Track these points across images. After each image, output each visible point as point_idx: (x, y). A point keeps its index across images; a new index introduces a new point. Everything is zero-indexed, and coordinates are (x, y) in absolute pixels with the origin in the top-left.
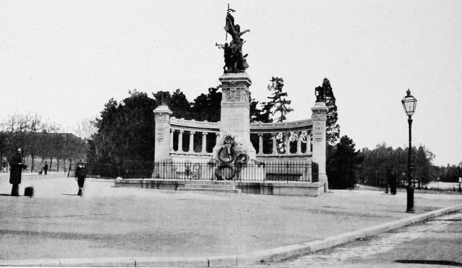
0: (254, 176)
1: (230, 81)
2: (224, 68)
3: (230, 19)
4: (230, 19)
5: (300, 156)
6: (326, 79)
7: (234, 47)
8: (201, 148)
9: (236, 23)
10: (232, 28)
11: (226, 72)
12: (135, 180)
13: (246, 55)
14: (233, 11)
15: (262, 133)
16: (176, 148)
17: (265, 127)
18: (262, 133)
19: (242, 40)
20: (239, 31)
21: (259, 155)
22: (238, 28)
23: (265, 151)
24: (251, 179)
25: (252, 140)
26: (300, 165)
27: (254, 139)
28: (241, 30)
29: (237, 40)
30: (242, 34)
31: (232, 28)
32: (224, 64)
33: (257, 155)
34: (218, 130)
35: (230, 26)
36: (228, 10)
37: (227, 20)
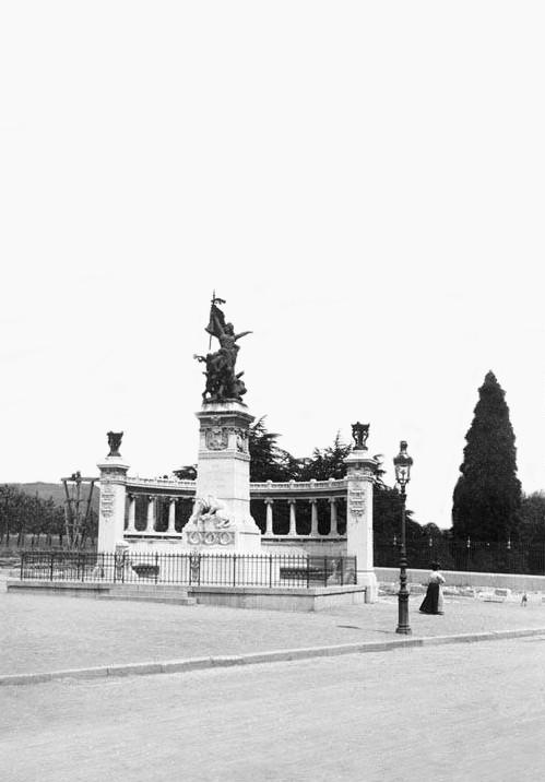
0: (219, 575)
1: (212, 417)
2: (204, 395)
3: (217, 315)
4: (217, 315)
5: (335, 540)
6: (490, 378)
7: (220, 361)
8: (146, 524)
9: (227, 321)
10: (218, 325)
11: (206, 402)
12: (352, 641)
13: (241, 374)
14: (221, 301)
15: (294, 499)
16: (141, 523)
17: (320, 488)
18: (294, 499)
19: (237, 348)
20: (232, 334)
21: (127, 533)
22: (229, 329)
23: (276, 531)
24: (228, 580)
25: (253, 513)
26: (289, 558)
27: (257, 509)
28: (237, 331)
29: (229, 351)
30: (239, 336)
31: (218, 325)
32: (204, 388)
33: (263, 536)
34: (194, 493)
35: (215, 324)
36: (213, 301)
37: (212, 318)
